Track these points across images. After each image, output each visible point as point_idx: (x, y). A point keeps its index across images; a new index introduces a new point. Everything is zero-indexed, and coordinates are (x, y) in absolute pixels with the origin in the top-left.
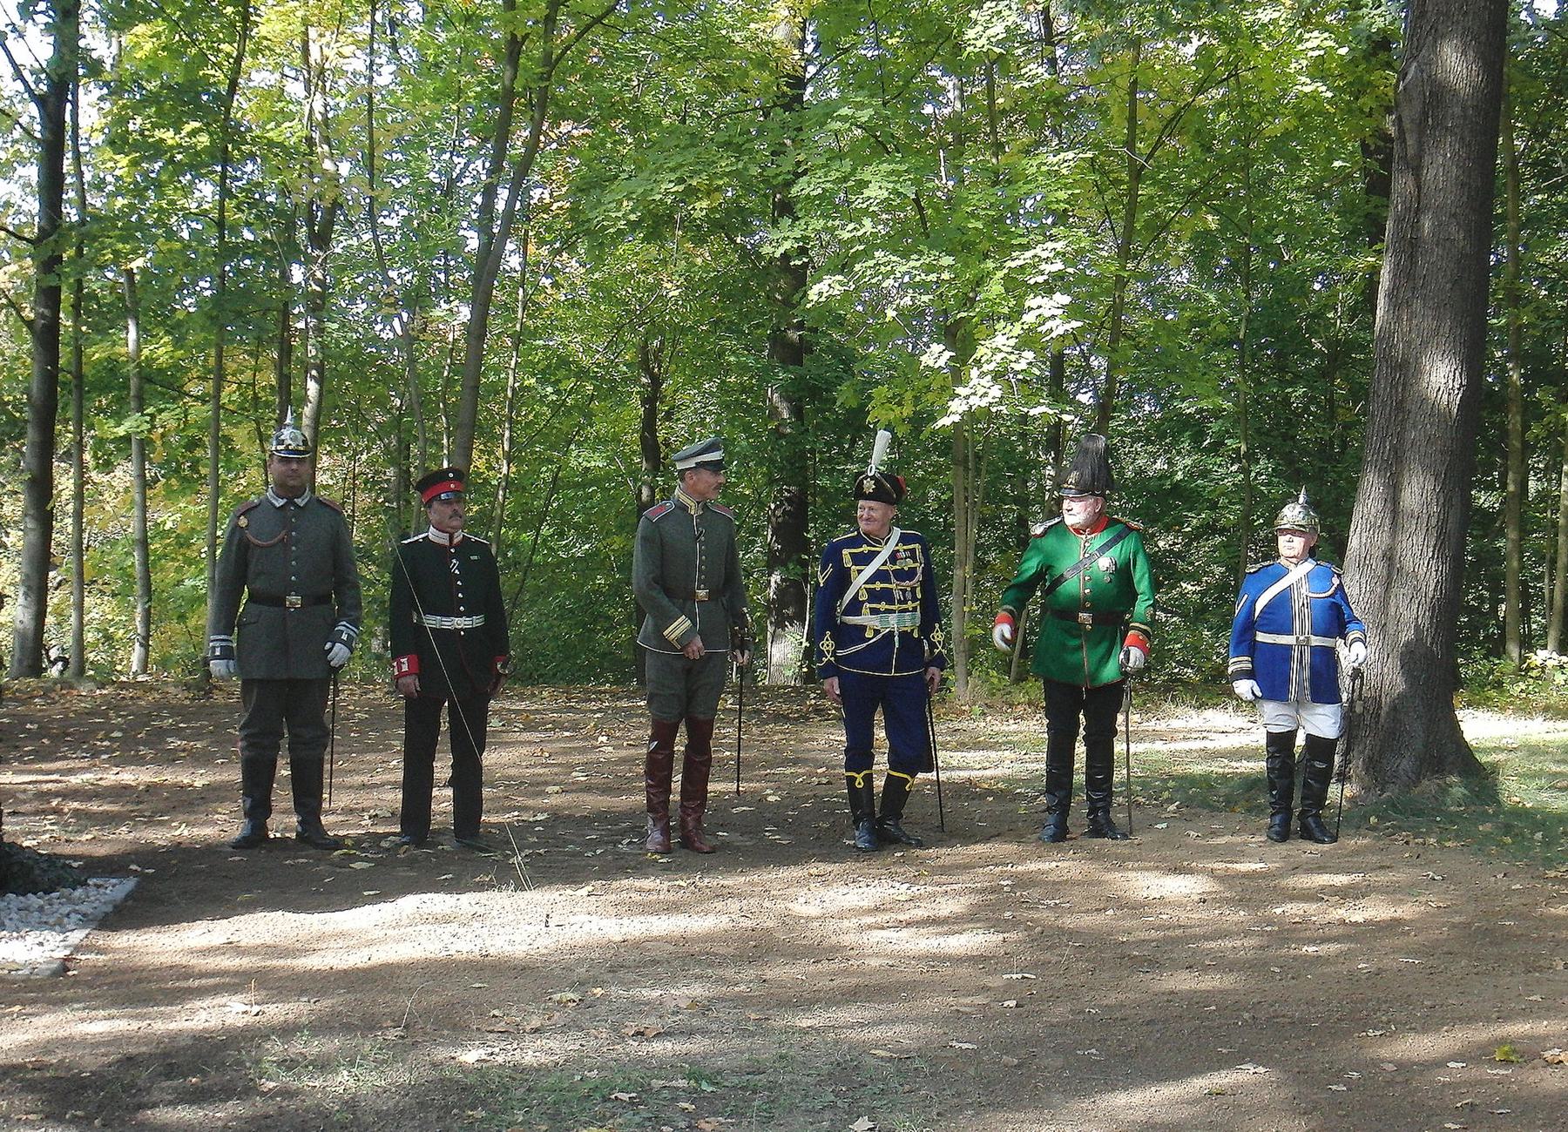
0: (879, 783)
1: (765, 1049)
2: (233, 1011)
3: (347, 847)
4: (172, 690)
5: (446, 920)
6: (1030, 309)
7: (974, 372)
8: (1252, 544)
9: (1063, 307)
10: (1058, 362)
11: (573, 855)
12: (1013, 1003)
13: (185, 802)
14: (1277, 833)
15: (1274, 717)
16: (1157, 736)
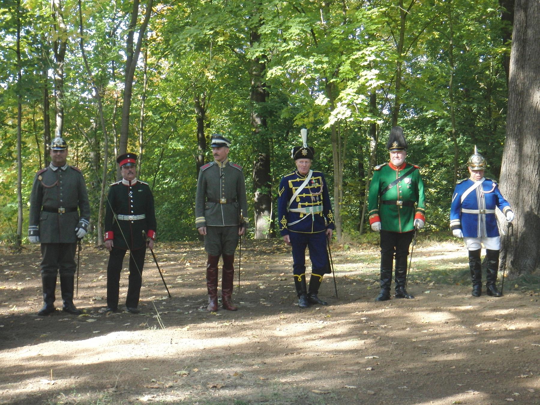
0: (308, 279)
1: (268, 391)
2: (43, 384)
3: (84, 313)
4: (4, 249)
5: (130, 342)
6: (362, 76)
7: (339, 104)
8: (459, 173)
9: (376, 75)
10: (373, 98)
11: (180, 313)
12: (370, 369)
13: (16, 297)
14: (476, 293)
15: (471, 244)
16: (422, 254)
